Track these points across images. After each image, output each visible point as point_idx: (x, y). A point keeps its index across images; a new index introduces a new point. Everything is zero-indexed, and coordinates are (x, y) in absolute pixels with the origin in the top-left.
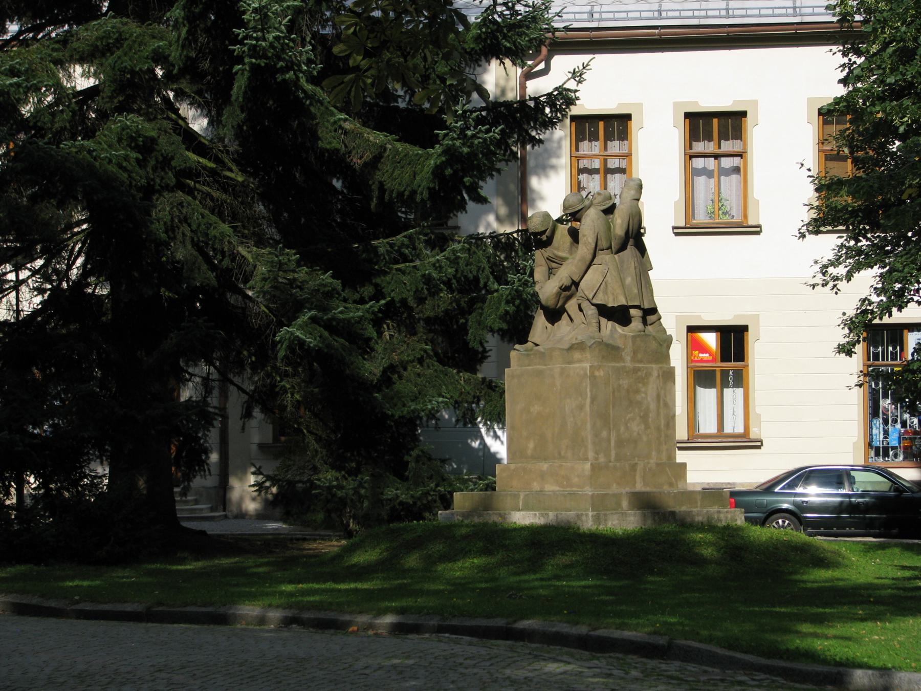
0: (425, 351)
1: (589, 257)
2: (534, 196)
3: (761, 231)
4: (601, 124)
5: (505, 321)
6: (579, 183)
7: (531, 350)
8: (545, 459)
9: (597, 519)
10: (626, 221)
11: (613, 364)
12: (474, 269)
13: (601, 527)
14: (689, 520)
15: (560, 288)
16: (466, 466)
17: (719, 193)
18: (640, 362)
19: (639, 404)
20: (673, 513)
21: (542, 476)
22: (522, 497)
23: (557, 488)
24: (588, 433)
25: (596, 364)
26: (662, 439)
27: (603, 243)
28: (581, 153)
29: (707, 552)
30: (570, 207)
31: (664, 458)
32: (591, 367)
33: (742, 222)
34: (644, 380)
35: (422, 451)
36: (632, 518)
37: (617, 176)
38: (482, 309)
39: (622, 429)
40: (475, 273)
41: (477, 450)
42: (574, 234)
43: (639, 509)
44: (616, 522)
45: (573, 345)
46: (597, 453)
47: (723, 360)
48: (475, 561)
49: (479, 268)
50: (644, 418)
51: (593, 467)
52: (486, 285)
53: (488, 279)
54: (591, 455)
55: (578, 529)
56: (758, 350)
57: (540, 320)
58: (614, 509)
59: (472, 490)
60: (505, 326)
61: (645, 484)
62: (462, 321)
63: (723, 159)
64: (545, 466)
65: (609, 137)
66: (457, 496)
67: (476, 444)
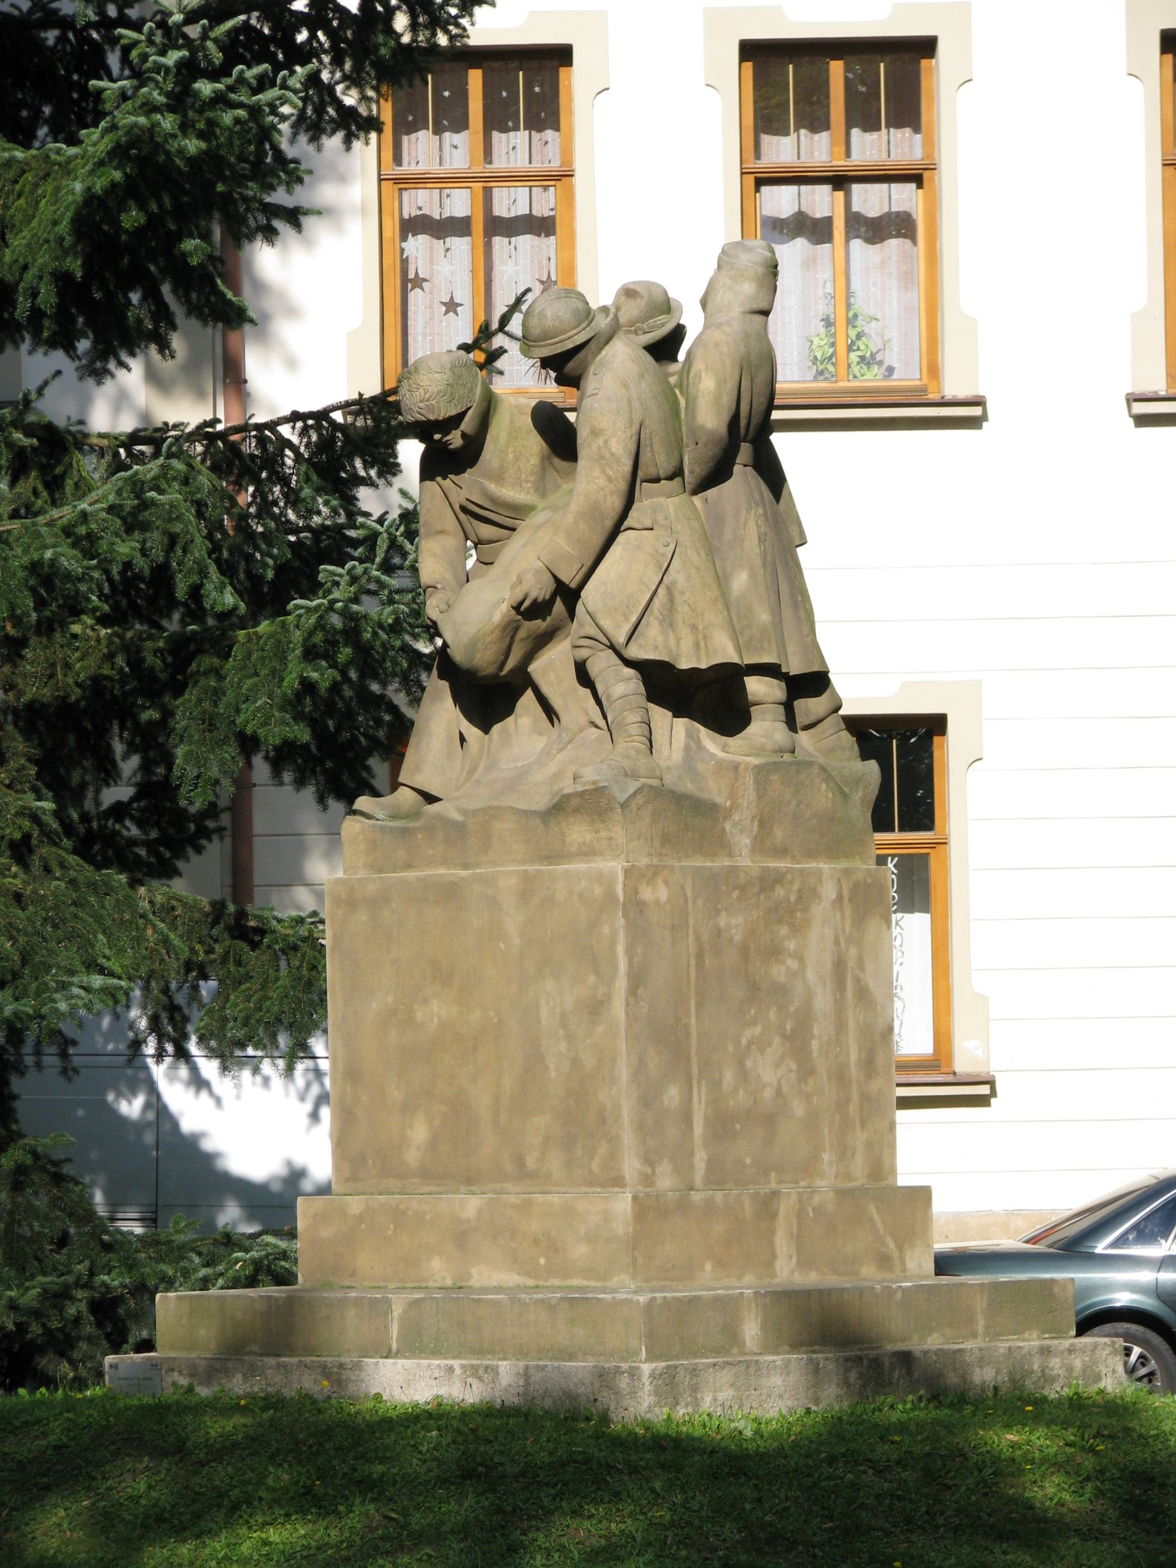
0: (35, 818)
1: (614, 503)
2: (268, 304)
3: (984, 417)
4: (475, 79)
5: (298, 717)
6: (405, 262)
7: (416, 814)
8: (470, 1180)
9: (668, 1384)
10: (731, 385)
11: (698, 862)
12: (155, 539)
13: (681, 1412)
14: (953, 1379)
15: (517, 608)
16: (101, 1179)
17: (849, 294)
18: (782, 852)
19: (781, 992)
20: (906, 1358)
21: (462, 1238)
22: (397, 1310)
23: (512, 1279)
24: (620, 1095)
25: (643, 861)
26: (853, 1108)
27: (658, 460)
28: (408, 167)
29: (1051, 1491)
30: (546, 336)
31: (859, 1167)
32: (627, 872)
33: (923, 390)
34: (793, 913)
35: (35, 1155)
36: (776, 1380)
37: (525, 241)
38: (221, 678)
39: (729, 1077)
40: (158, 555)
41: (138, 1127)
42: (558, 435)
43: (795, 1346)
44: (726, 1394)
45: (567, 797)
46: (649, 1161)
48: (273, 1535)
49: (173, 539)
50: (797, 1041)
51: (644, 1209)
52: (196, 592)
53: (203, 573)
54: (631, 1166)
55: (605, 1419)
56: (972, 786)
57: (439, 716)
58: (717, 1351)
59: (205, 1284)
60: (302, 733)
61: (805, 1262)
62: (150, 715)
63: (856, 188)
64: (470, 1205)
65: (499, 118)
66: (167, 1303)
67: (132, 1107)
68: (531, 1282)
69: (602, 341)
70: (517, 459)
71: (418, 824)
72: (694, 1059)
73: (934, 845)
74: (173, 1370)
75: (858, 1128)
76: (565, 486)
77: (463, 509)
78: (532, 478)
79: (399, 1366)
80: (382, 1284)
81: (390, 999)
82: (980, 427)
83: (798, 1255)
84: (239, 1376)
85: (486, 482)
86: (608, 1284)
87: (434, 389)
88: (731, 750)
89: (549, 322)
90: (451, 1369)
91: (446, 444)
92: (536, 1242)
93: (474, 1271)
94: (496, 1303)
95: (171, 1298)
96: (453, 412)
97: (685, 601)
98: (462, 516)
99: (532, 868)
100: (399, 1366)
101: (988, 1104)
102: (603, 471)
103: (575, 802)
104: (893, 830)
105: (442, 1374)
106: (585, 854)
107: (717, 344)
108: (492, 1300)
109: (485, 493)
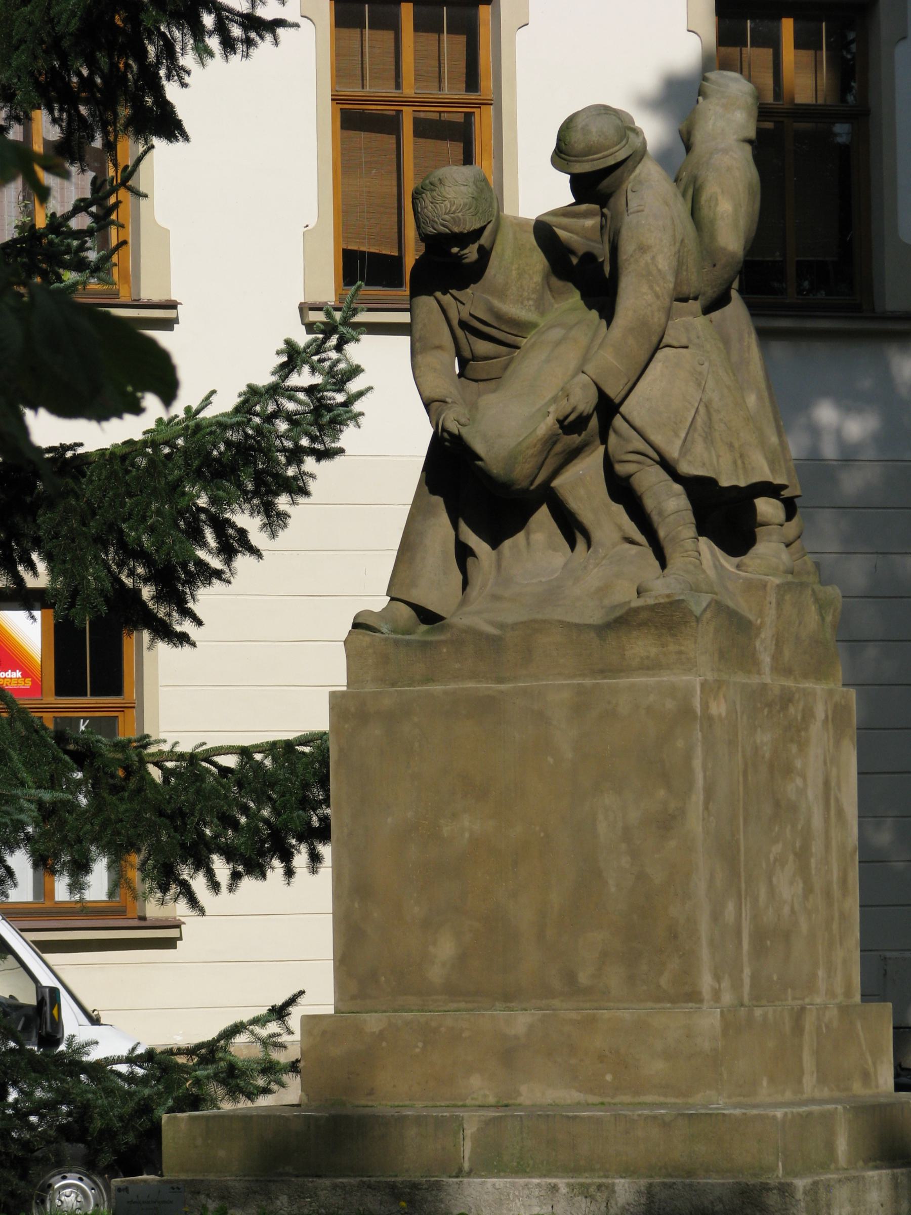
3: (176, 321)
8: (509, 997)
21: (508, 1055)
22: (470, 1129)
26: (835, 926)
46: (717, 978)
47: (62, 689)
64: (520, 1022)
68: (592, 1099)
69: (638, 159)
70: (520, 276)
71: (442, 637)
72: (743, 874)
73: (122, 709)
74: (199, 1193)
75: (838, 946)
76: (556, 306)
77: (463, 325)
78: (534, 296)
79: (489, 1185)
80: (407, 1103)
81: (410, 814)
82: (172, 329)
83: (818, 1072)
84: (284, 1199)
85: (490, 298)
86: (691, 1101)
87: (460, 201)
88: (750, 569)
89: (594, 138)
90: (554, 1188)
91: (461, 258)
92: (601, 1058)
93: (524, 1089)
94: (598, 1121)
95: (182, 1119)
96: (477, 226)
97: (721, 420)
98: (459, 332)
99: (588, 682)
100: (489, 1185)
101: (174, 947)
102: (651, 288)
103: (644, 615)
104: (86, 695)
105: (543, 1193)
106: (648, 668)
107: (729, 169)
108: (590, 1117)
109: (491, 310)
